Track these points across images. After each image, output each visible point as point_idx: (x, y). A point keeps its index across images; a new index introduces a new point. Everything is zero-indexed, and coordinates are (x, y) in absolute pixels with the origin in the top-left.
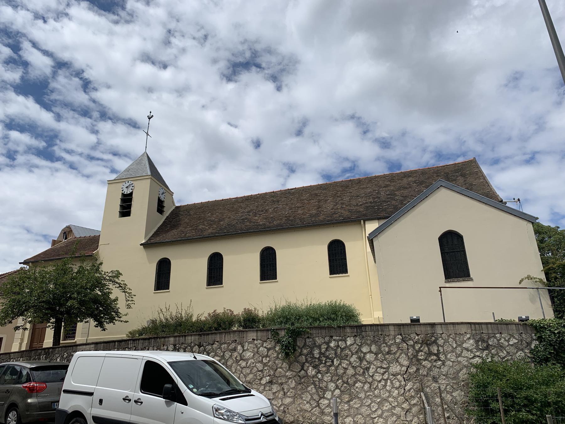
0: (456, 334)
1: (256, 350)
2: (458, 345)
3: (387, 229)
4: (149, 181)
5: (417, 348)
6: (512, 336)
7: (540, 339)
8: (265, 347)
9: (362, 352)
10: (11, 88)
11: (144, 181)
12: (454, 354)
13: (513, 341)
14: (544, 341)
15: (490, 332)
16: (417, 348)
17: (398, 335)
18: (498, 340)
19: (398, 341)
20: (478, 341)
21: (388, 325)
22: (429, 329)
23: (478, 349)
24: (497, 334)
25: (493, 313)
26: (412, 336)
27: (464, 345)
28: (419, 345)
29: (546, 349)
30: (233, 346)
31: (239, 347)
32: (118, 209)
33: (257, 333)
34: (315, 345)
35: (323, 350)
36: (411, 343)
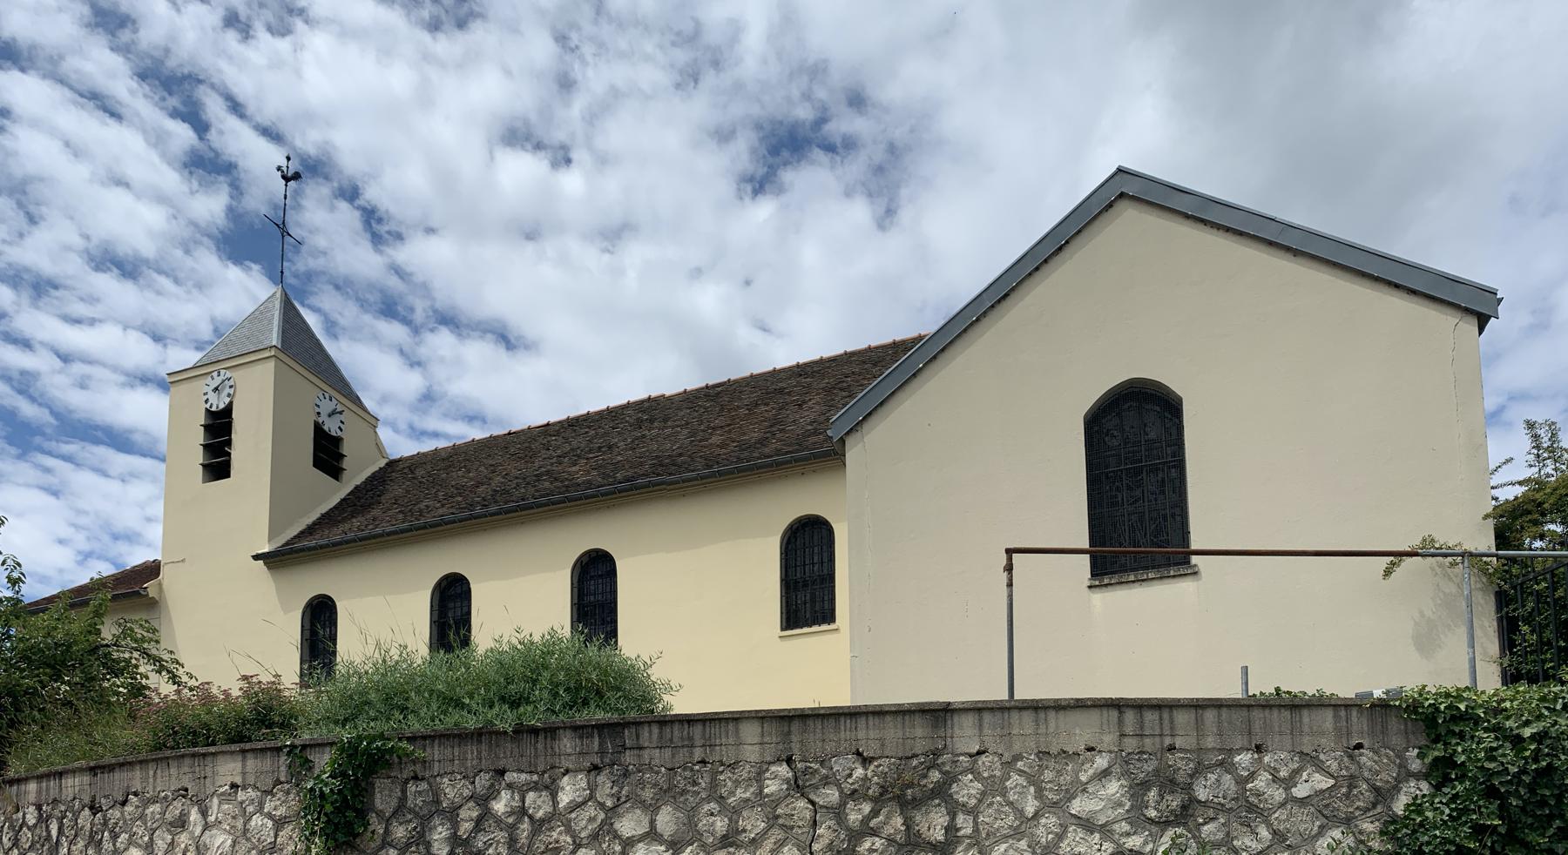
0: (1043, 754)
1: (240, 824)
2: (1047, 806)
3: (900, 396)
4: (271, 364)
5: (854, 817)
6: (1311, 760)
7: (1441, 772)
8: (270, 816)
9: (616, 836)
10: (205, 239)
11: (259, 367)
12: (1023, 844)
13: (1312, 783)
14: (1462, 778)
15: (1210, 742)
16: (854, 817)
17: (778, 760)
18: (1241, 782)
19: (771, 787)
20: (1145, 786)
21: (736, 718)
22: (919, 732)
23: (1137, 819)
24: (1239, 751)
25: (1245, 670)
26: (838, 765)
27: (1076, 806)
28: (867, 808)
29: (1466, 811)
30: (176, 809)
31: (194, 815)
32: (199, 456)
33: (244, 758)
34: (437, 808)
35: (465, 827)
36: (831, 795)
